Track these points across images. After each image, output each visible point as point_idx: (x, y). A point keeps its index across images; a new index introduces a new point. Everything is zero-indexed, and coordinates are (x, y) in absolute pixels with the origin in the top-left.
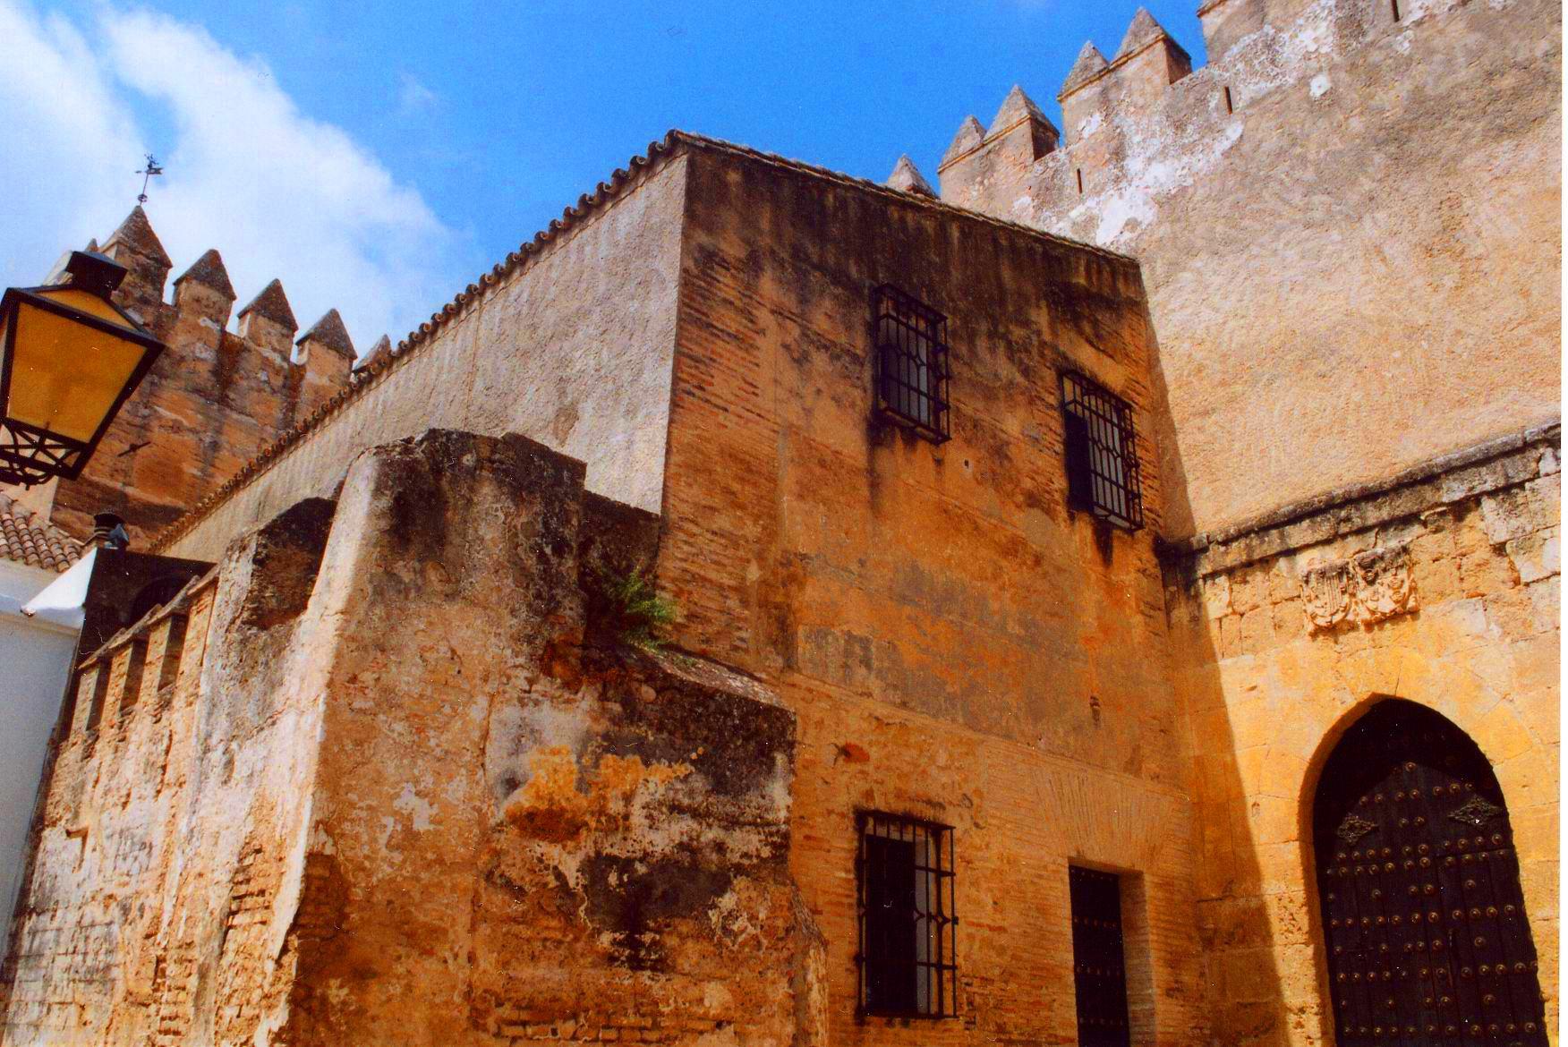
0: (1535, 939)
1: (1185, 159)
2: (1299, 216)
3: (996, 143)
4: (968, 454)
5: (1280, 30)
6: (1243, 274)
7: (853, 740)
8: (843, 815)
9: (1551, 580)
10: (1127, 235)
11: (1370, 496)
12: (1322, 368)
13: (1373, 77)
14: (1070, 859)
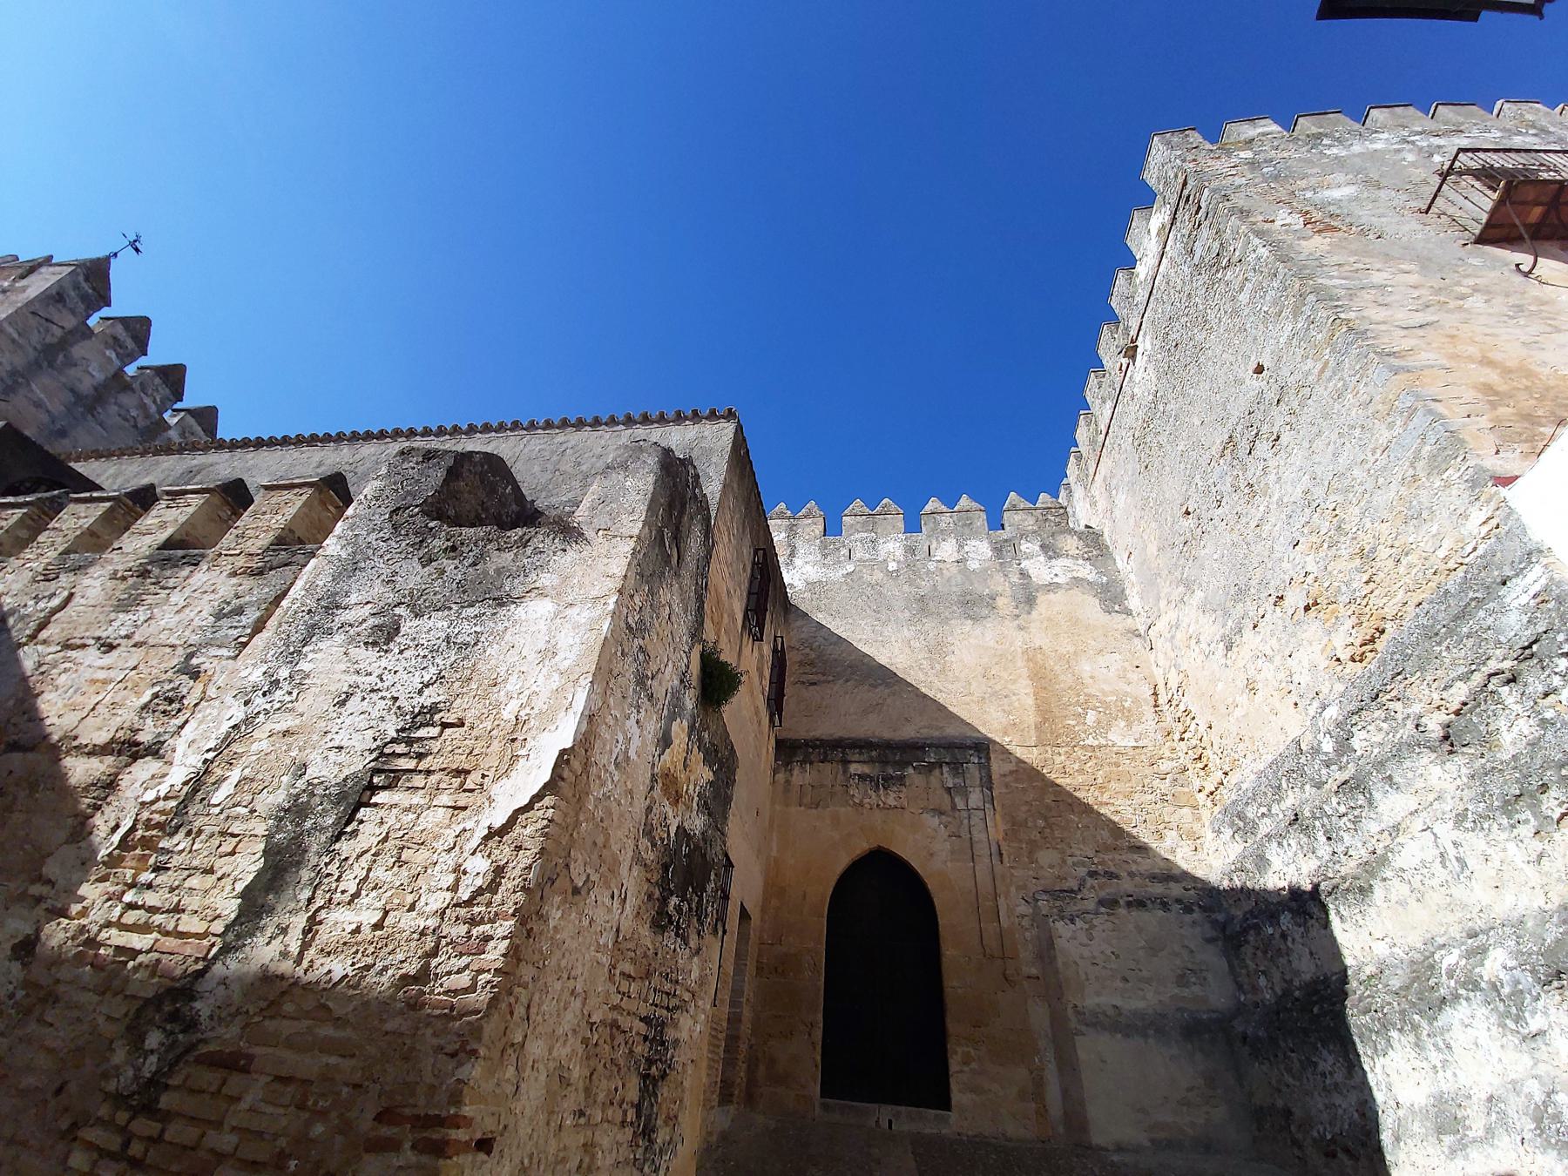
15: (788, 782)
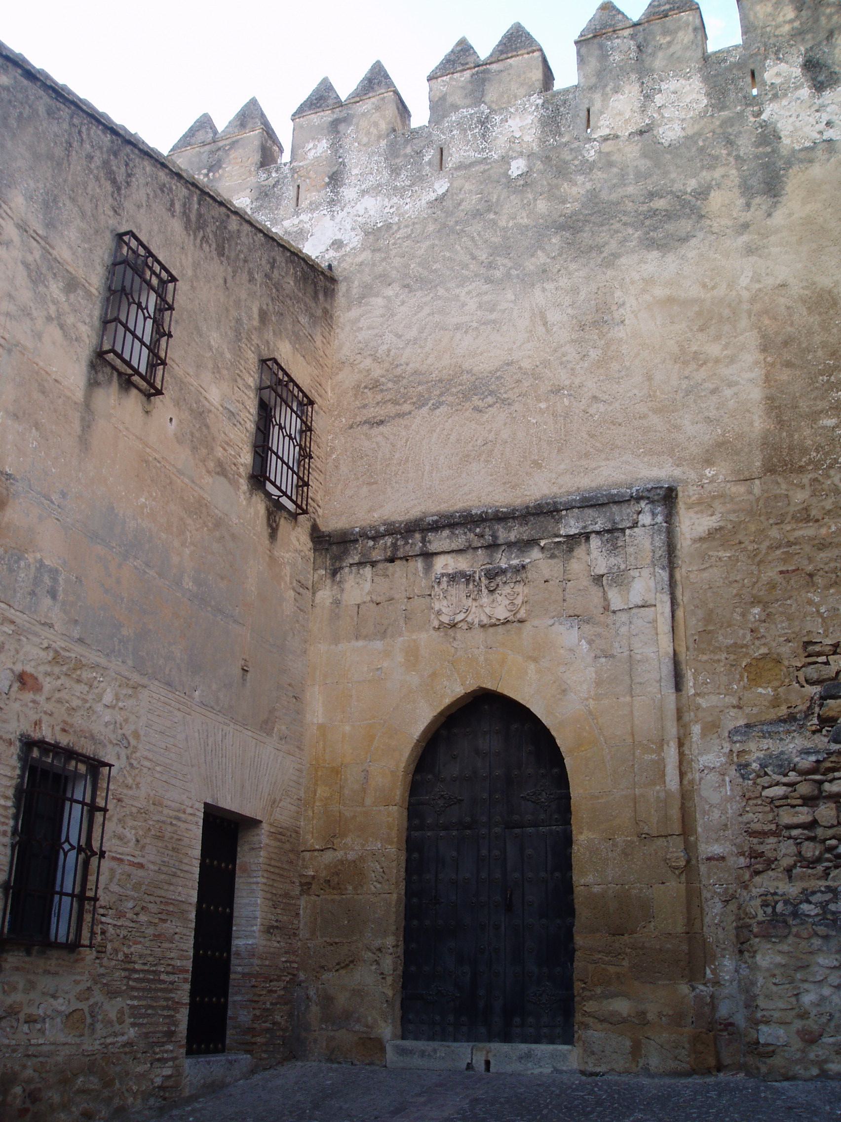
0: (576, 901)
1: (395, 200)
2: (482, 271)
3: (227, 142)
4: (172, 412)
5: (492, 111)
6: (427, 310)
7: (29, 669)
8: (10, 743)
9: (634, 611)
10: (332, 254)
11: (501, 518)
12: (481, 404)
13: (562, 171)
14: (206, 804)
15: (337, 602)
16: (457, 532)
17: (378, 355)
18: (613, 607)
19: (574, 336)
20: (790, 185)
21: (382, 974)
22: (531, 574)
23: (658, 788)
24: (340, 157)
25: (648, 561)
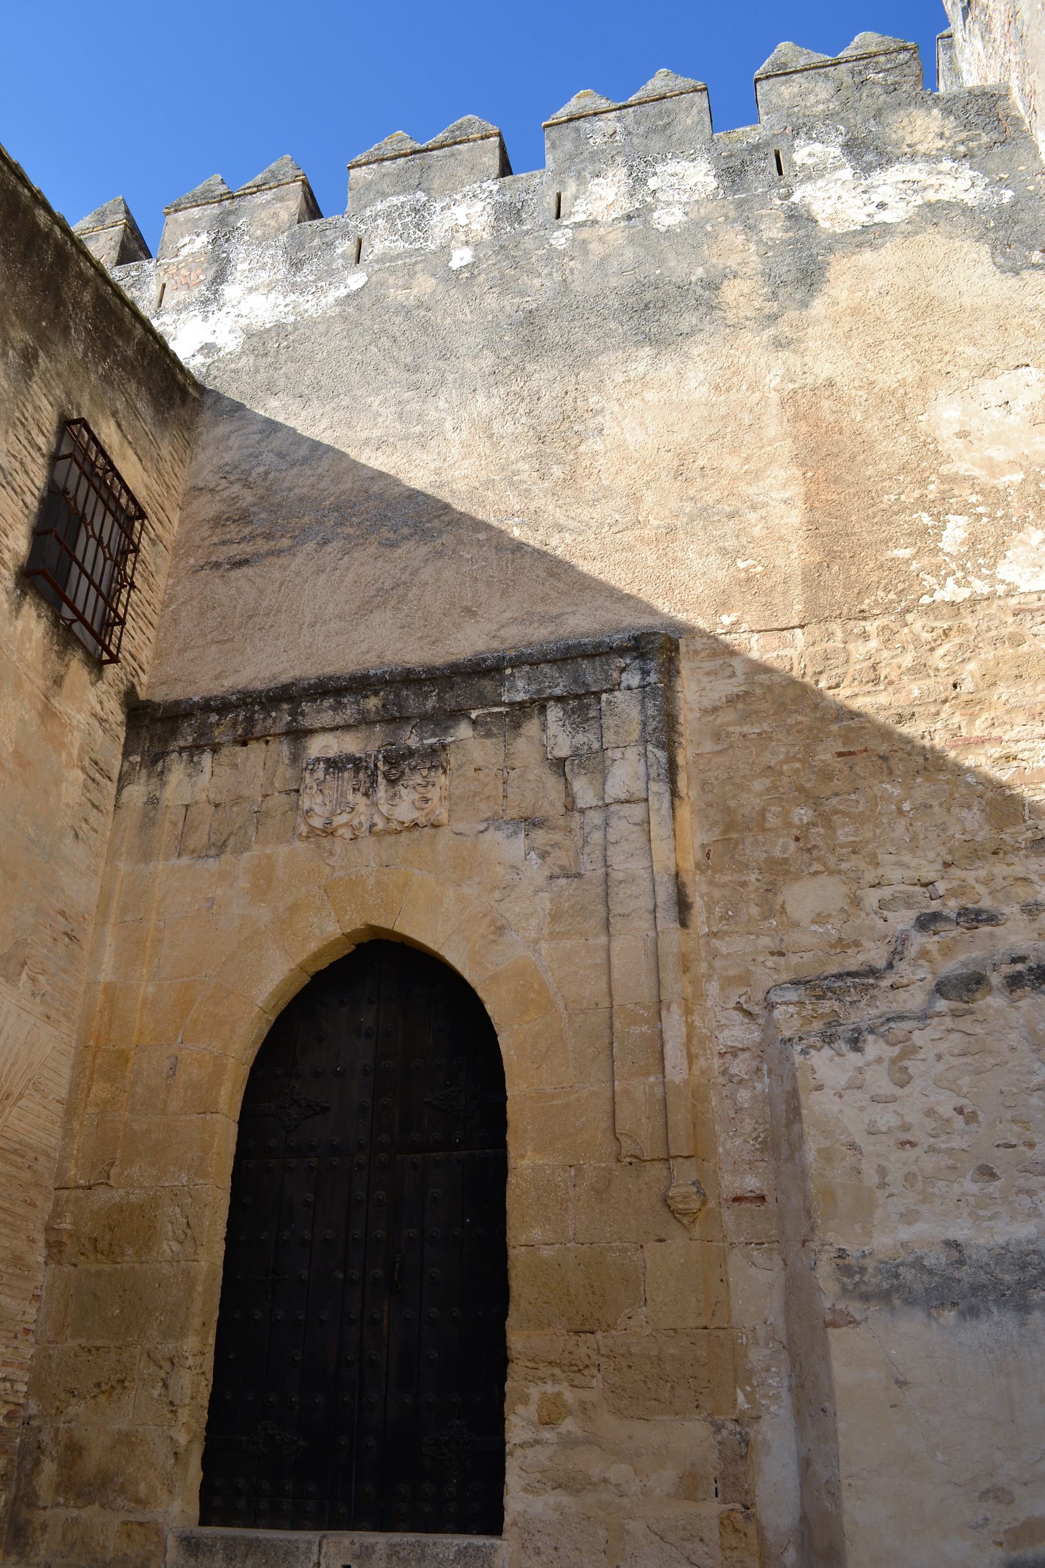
15: (153, 802)
16: (345, 700)
17: (250, 479)
18: (580, 804)
19: (531, 450)
20: (832, 271)
21: (171, 1403)
22: (453, 759)
23: (652, 1079)
24: (223, 252)
25: (635, 735)
